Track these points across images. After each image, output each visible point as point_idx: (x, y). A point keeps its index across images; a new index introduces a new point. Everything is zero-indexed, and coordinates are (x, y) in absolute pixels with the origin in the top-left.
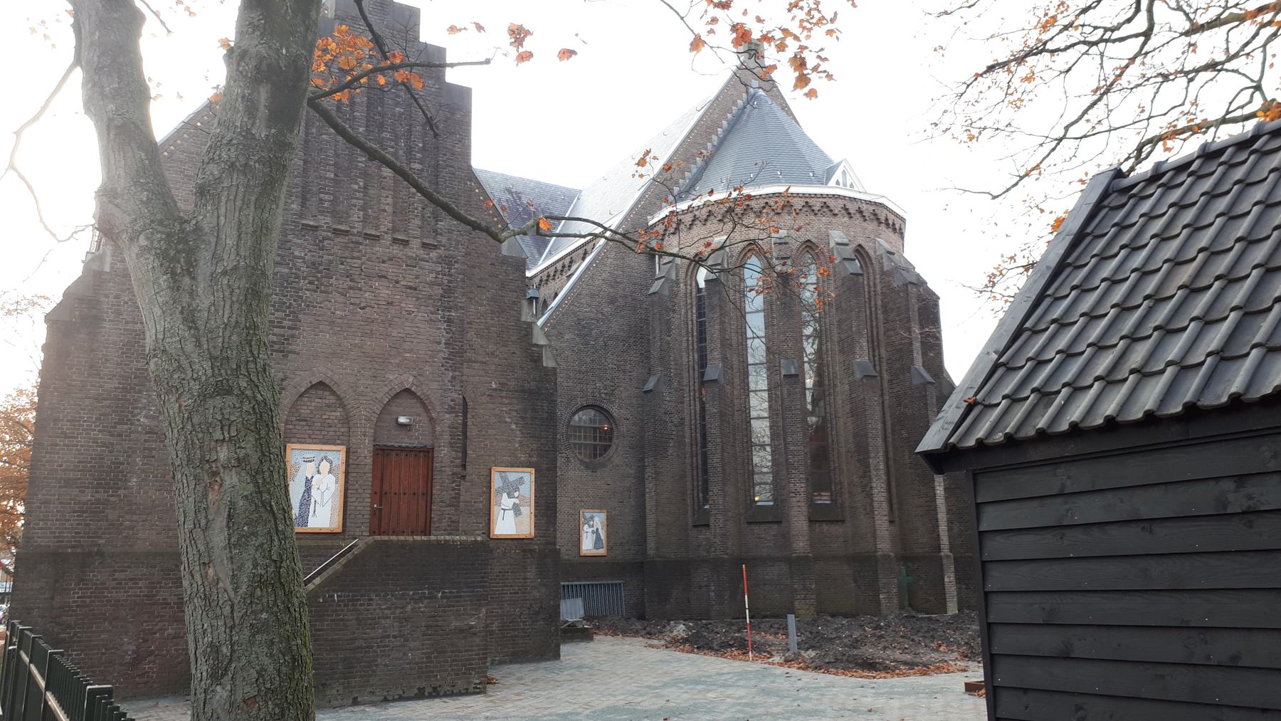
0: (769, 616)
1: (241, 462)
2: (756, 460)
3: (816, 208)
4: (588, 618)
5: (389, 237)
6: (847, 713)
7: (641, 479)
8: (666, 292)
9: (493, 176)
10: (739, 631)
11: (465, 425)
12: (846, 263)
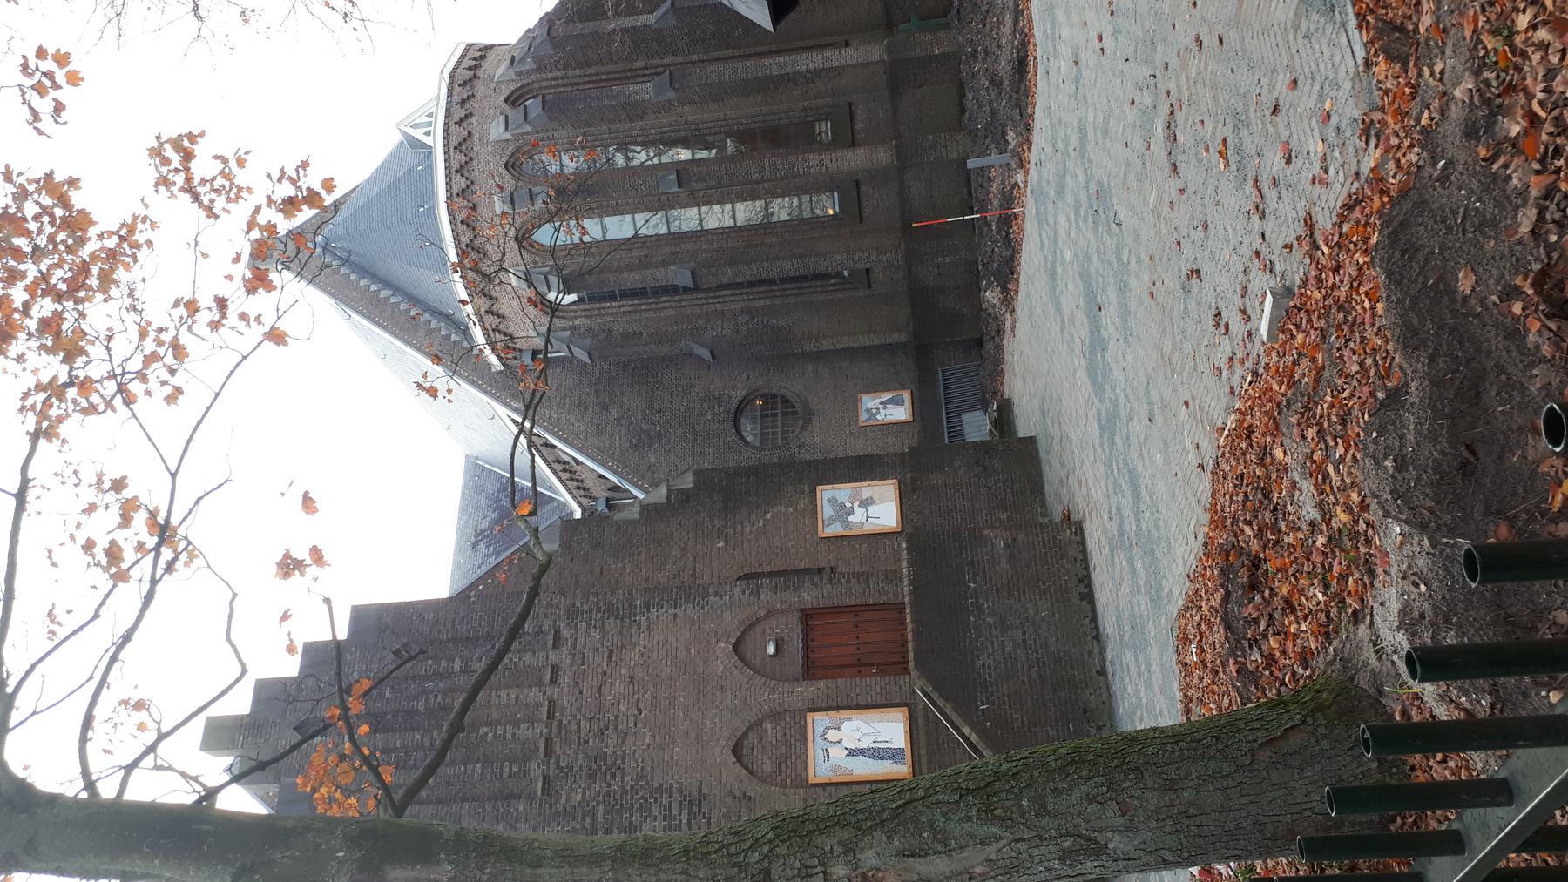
0: (969, 190)
1: (849, 849)
2: (784, 216)
3: (464, 159)
4: (985, 406)
5: (549, 690)
6: (1080, 91)
7: (819, 356)
8: (588, 341)
9: (457, 566)
10: (989, 225)
11: (771, 574)
12: (530, 117)
